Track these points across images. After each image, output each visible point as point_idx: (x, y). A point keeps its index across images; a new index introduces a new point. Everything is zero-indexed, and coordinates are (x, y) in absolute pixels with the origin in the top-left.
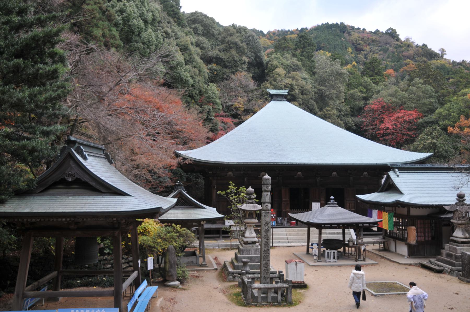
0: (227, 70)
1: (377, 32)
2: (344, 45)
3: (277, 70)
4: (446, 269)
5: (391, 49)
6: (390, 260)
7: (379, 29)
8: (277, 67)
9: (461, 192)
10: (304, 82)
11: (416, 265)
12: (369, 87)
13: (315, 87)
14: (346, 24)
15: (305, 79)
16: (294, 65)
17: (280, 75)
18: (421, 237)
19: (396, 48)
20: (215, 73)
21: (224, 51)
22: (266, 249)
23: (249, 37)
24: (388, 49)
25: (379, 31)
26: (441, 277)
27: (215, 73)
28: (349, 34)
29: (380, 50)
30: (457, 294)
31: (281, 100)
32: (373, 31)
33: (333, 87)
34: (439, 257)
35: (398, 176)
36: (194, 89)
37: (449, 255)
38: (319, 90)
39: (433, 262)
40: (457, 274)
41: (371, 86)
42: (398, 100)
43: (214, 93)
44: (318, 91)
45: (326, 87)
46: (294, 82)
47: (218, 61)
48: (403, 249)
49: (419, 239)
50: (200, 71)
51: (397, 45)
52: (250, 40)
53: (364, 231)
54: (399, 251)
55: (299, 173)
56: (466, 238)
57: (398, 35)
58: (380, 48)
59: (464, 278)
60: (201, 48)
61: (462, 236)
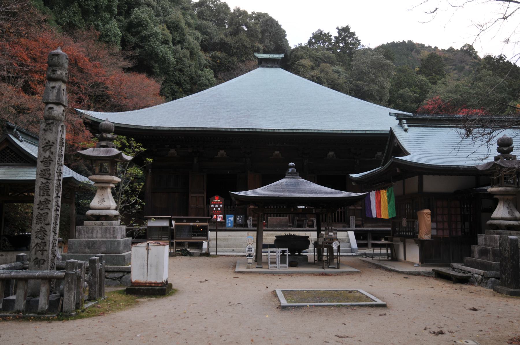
0: (235, 59)
1: (451, 50)
2: (411, 64)
3: (303, 61)
4: (476, 275)
5: (467, 67)
6: (391, 271)
7: (453, 47)
8: (302, 57)
9: (505, 135)
10: (336, 76)
11: (427, 275)
12: (425, 87)
13: (351, 82)
14: (415, 42)
15: (338, 72)
16: (325, 58)
17: (304, 66)
18: (443, 229)
19: (473, 66)
20: (218, 61)
21: (231, 35)
22: (43, 199)
23: (267, 21)
24: (464, 68)
25: (453, 49)
26: (461, 289)
27: (218, 61)
28: (418, 52)
29: (455, 69)
30: (475, 310)
31: (272, 67)
32: (446, 49)
33: (373, 81)
34: (467, 259)
35: (406, 130)
36: (183, 74)
37: (484, 253)
38: (357, 86)
39: (459, 268)
40: (493, 283)
41: (428, 86)
42: (458, 96)
43: (209, 80)
44: (355, 88)
45: (365, 82)
46: (322, 75)
47: (223, 46)
48: (413, 254)
49: (440, 233)
50: (192, 53)
51: (475, 62)
52: (268, 25)
53: (374, 240)
54: (409, 258)
55: (277, 152)
56: (516, 219)
57: (477, 52)
58: (454, 67)
59: (504, 288)
60: (203, 33)
61: (507, 216)
